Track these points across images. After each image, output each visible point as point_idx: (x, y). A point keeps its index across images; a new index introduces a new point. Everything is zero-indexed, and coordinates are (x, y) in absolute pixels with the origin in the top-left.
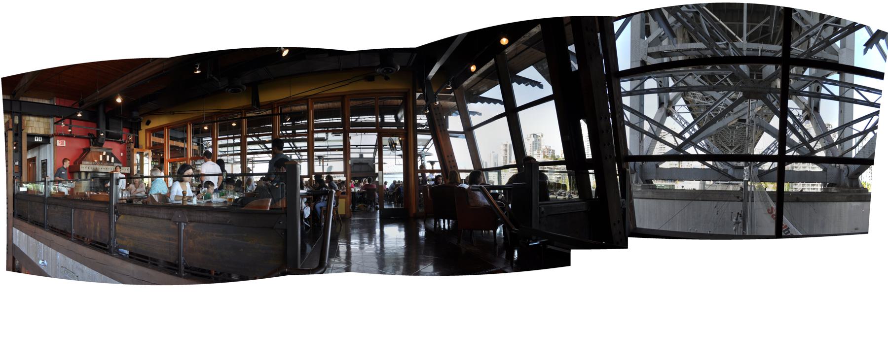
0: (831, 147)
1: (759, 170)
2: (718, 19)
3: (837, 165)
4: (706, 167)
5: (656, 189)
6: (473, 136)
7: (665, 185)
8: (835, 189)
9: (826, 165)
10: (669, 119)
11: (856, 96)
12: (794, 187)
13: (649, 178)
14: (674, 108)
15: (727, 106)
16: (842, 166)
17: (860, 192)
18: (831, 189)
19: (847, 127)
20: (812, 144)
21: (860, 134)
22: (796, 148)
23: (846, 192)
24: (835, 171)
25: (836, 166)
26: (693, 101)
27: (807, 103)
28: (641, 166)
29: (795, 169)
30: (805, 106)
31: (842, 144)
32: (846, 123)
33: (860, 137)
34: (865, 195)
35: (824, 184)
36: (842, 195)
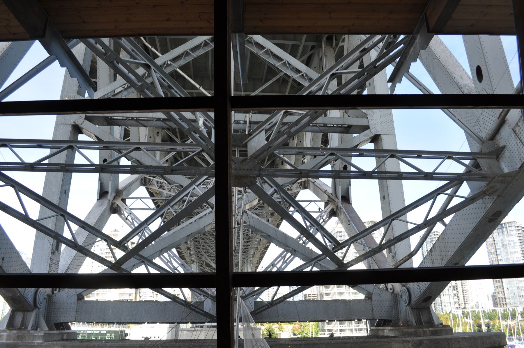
0: (374, 254)
1: (256, 303)
2: (198, 86)
3: (390, 285)
4: (162, 298)
5: (75, 339)
6: (440, 269)
7: (109, 332)
8: (390, 330)
9: (370, 287)
10: (114, 217)
11: (404, 168)
12: (327, 327)
13: (62, 320)
14: (124, 200)
15: (182, 186)
16: (398, 286)
17: (436, 333)
18: (383, 330)
19: (394, 220)
20: (339, 254)
21: (418, 228)
22: (313, 262)
23: (410, 335)
24: (387, 297)
25: (387, 289)
26: (161, 194)
27: (330, 191)
28: (50, 297)
29: (325, 298)
30: (329, 196)
31: (392, 247)
32: (392, 213)
33: (423, 232)
34: (448, 339)
35: (372, 321)
36: (404, 341)
